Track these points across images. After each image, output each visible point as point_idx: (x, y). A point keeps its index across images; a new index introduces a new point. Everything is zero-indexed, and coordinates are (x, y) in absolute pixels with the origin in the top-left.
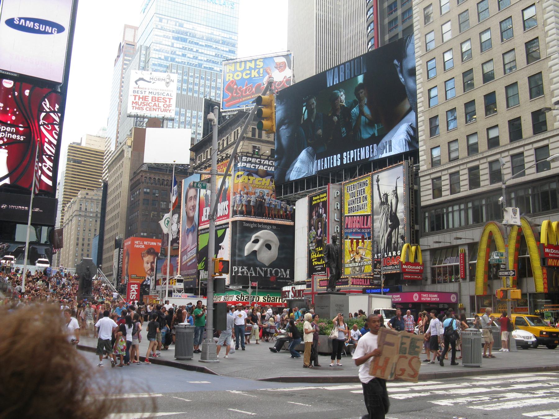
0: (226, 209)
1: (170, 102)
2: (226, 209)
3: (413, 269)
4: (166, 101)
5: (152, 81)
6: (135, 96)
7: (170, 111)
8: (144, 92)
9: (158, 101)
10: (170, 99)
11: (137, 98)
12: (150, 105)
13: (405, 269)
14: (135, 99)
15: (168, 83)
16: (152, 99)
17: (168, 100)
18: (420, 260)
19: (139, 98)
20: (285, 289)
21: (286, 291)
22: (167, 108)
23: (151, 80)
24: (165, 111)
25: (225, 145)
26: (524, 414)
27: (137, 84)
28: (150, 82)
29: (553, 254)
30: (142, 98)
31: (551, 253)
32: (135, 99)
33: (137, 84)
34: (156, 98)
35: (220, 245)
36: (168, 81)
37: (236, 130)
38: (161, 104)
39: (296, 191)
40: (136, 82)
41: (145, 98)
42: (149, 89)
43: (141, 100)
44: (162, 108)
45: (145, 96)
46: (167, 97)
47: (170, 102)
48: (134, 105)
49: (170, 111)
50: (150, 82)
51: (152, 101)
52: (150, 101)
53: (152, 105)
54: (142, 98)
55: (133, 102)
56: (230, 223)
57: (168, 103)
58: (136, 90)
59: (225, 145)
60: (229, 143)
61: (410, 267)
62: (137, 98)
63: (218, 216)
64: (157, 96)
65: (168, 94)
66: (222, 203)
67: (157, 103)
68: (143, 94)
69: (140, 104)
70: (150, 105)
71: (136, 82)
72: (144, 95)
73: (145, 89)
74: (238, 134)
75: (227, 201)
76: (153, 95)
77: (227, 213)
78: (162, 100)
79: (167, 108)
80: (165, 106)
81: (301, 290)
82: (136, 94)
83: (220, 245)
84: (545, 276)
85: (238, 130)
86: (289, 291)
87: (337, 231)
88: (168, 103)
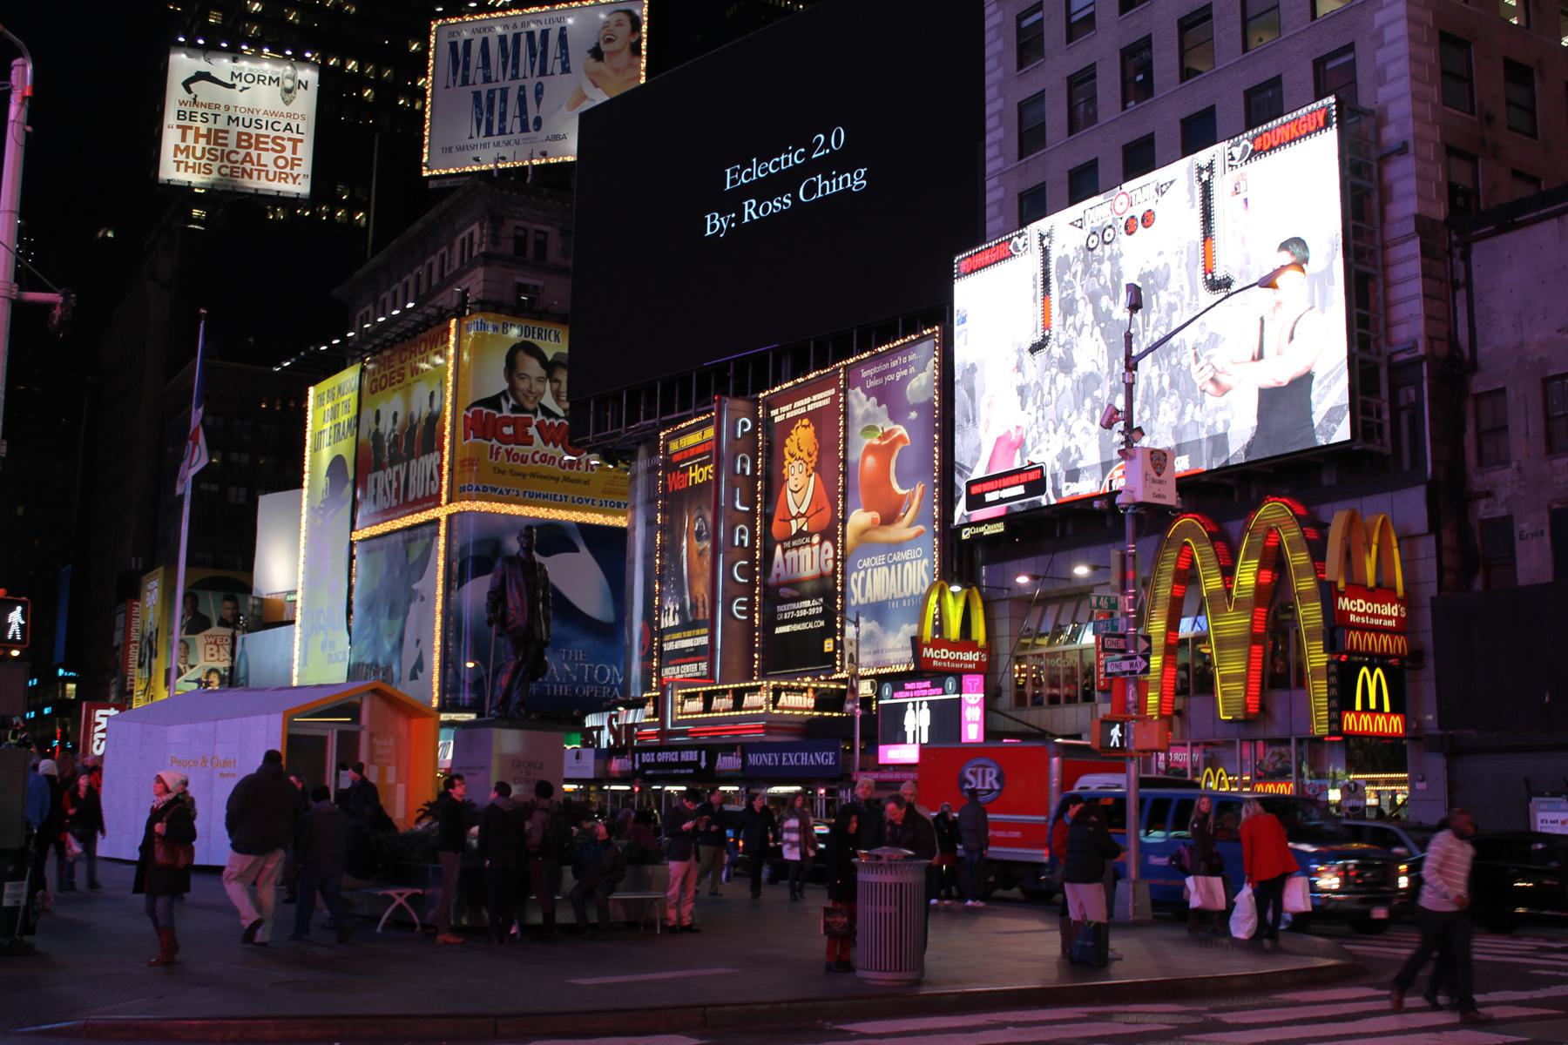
0: (432, 478)
1: (294, 152)
2: (432, 478)
3: (955, 661)
4: (284, 148)
5: (240, 85)
6: (184, 129)
7: (295, 179)
8: (211, 118)
9: (257, 148)
10: (295, 142)
11: (191, 134)
12: (233, 157)
13: (931, 659)
14: (184, 139)
15: (289, 91)
16: (239, 140)
17: (289, 145)
18: (979, 632)
19: (197, 136)
20: (591, 721)
21: (593, 728)
22: (287, 170)
23: (236, 81)
24: (280, 177)
25: (435, 281)
26: (798, 788)
27: (189, 91)
28: (233, 86)
29: (1365, 614)
30: (208, 136)
31: (1357, 613)
32: (184, 139)
33: (189, 91)
34: (250, 136)
35: (415, 586)
36: (289, 84)
37: (465, 234)
38: (268, 158)
39: (633, 418)
40: (187, 85)
41: (217, 138)
42: (227, 108)
43: (202, 141)
44: (272, 169)
45: (217, 131)
46: (288, 134)
47: (294, 152)
48: (181, 157)
49: (295, 179)
50: (233, 86)
51: (239, 146)
52: (232, 146)
53: (240, 158)
54: (208, 136)
55: (177, 147)
56: (443, 519)
57: (288, 154)
58: (188, 109)
59: (435, 281)
60: (447, 273)
61: (945, 653)
62: (191, 134)
63: (411, 497)
64: (253, 131)
65: (288, 127)
66: (421, 459)
67: (254, 154)
68: (211, 125)
69: (199, 154)
70: (233, 157)
71: (187, 85)
72: (214, 127)
73: (217, 106)
74: (471, 244)
75: (437, 454)
76: (241, 129)
77: (434, 491)
78: (271, 145)
79: (287, 170)
80: (281, 162)
81: (634, 725)
82: (187, 123)
83: (415, 586)
84: (1334, 691)
85: (471, 235)
86: (600, 729)
87: (742, 542)
88: (288, 154)
